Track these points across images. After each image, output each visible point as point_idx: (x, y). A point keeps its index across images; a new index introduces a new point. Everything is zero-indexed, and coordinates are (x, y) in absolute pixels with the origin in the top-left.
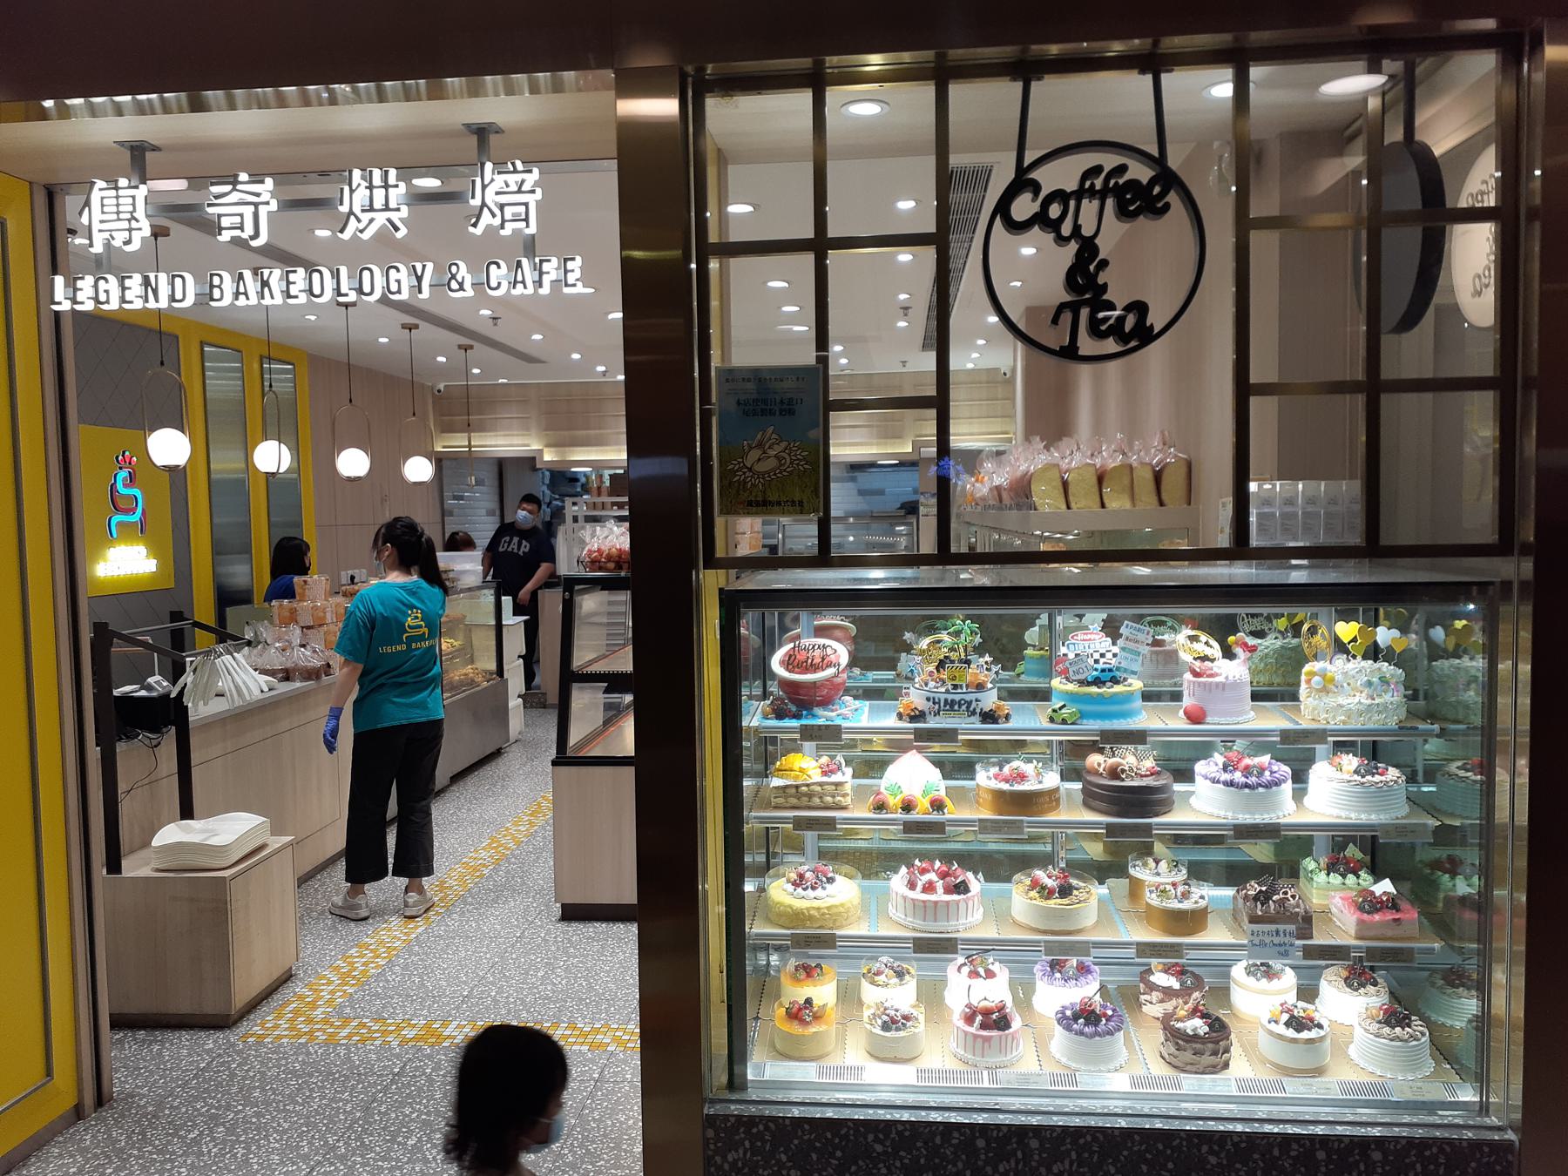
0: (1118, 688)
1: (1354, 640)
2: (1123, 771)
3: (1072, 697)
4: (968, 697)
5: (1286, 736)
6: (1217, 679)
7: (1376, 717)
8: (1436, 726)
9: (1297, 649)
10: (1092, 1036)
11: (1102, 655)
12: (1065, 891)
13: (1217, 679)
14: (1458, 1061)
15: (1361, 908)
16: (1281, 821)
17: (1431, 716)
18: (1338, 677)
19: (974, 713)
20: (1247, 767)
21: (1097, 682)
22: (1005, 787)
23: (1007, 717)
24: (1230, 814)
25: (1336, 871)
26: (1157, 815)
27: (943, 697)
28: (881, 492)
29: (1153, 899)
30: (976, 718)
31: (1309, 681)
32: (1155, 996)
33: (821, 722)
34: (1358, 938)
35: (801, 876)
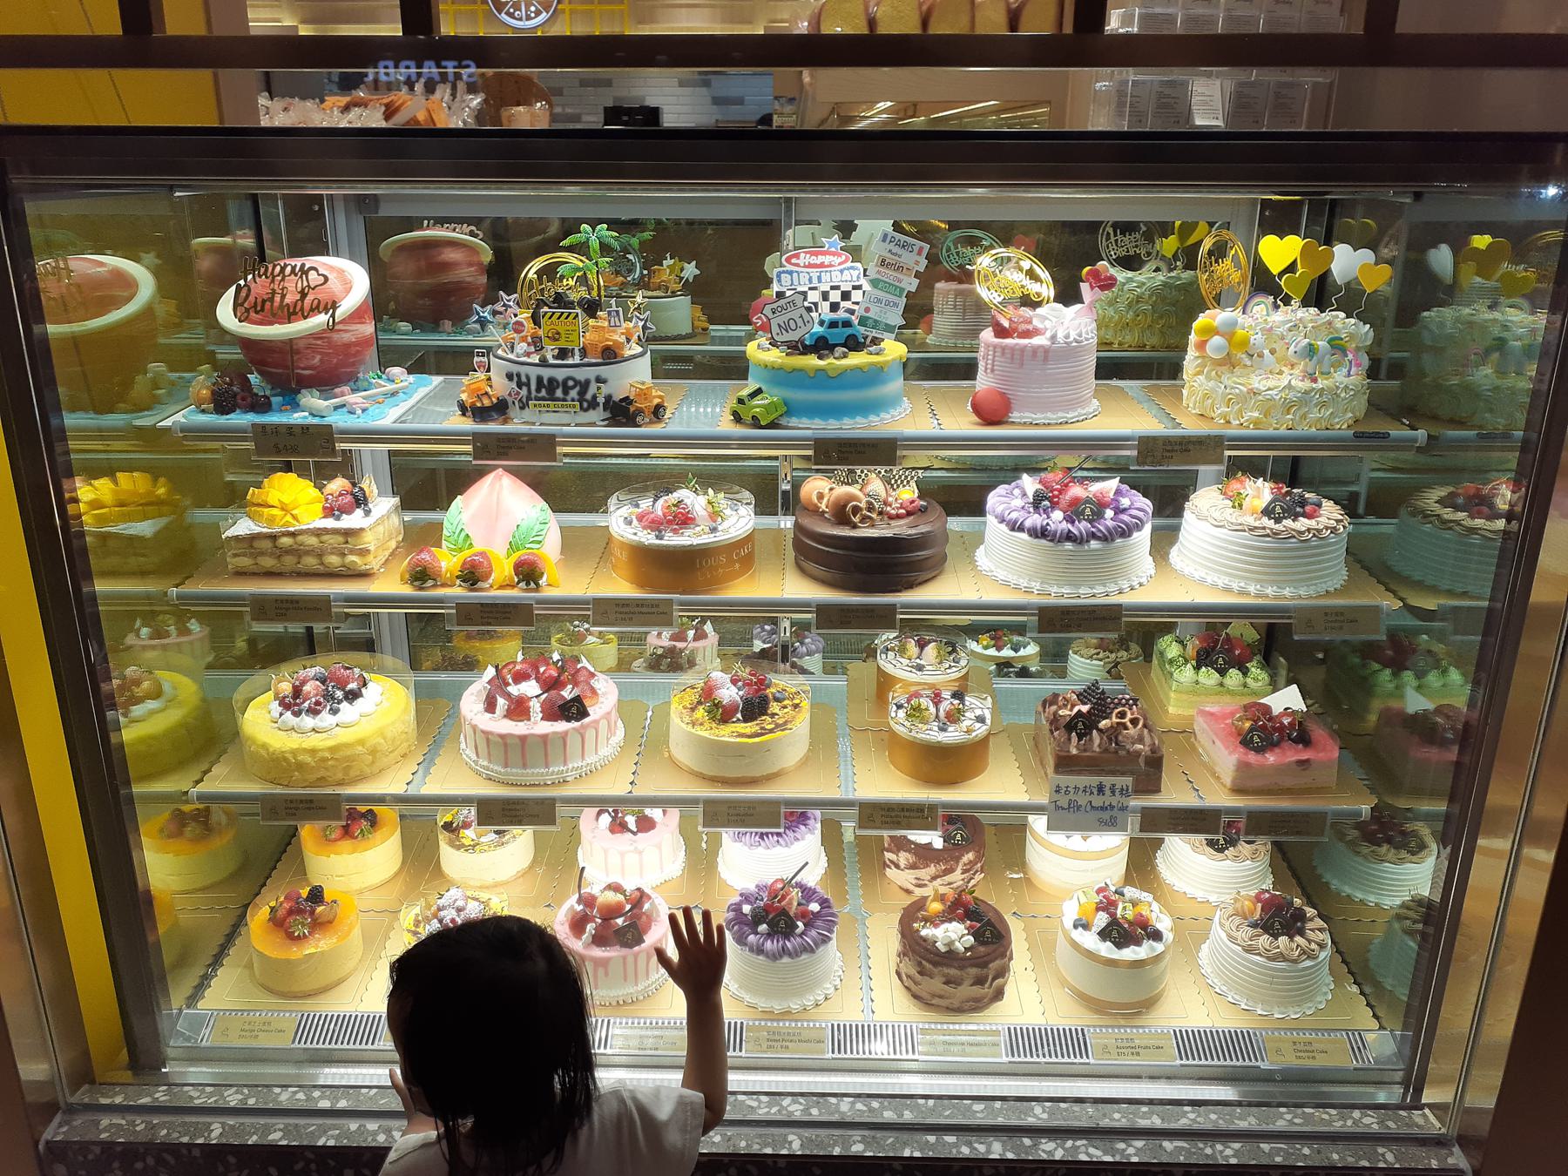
0: (856, 359)
1: (1291, 268)
2: (856, 510)
3: (778, 375)
4: (581, 374)
5: (1150, 447)
6: (1037, 341)
7: (1315, 414)
8: (1421, 434)
9: (1191, 288)
10: (774, 957)
11: (846, 296)
12: (755, 708)
13: (1037, 341)
14: (1377, 985)
15: (1246, 742)
16: (1128, 599)
17: (1409, 411)
18: (1257, 339)
19: (593, 404)
20: (1076, 502)
21: (821, 346)
22: (648, 538)
23: (658, 412)
24: (1036, 586)
25: (1211, 664)
26: (910, 586)
27: (534, 372)
28: (740, 101)
29: (898, 720)
30: (597, 415)
31: (1201, 345)
32: (904, 858)
33: (298, 418)
34: (1238, 790)
35: (297, 692)
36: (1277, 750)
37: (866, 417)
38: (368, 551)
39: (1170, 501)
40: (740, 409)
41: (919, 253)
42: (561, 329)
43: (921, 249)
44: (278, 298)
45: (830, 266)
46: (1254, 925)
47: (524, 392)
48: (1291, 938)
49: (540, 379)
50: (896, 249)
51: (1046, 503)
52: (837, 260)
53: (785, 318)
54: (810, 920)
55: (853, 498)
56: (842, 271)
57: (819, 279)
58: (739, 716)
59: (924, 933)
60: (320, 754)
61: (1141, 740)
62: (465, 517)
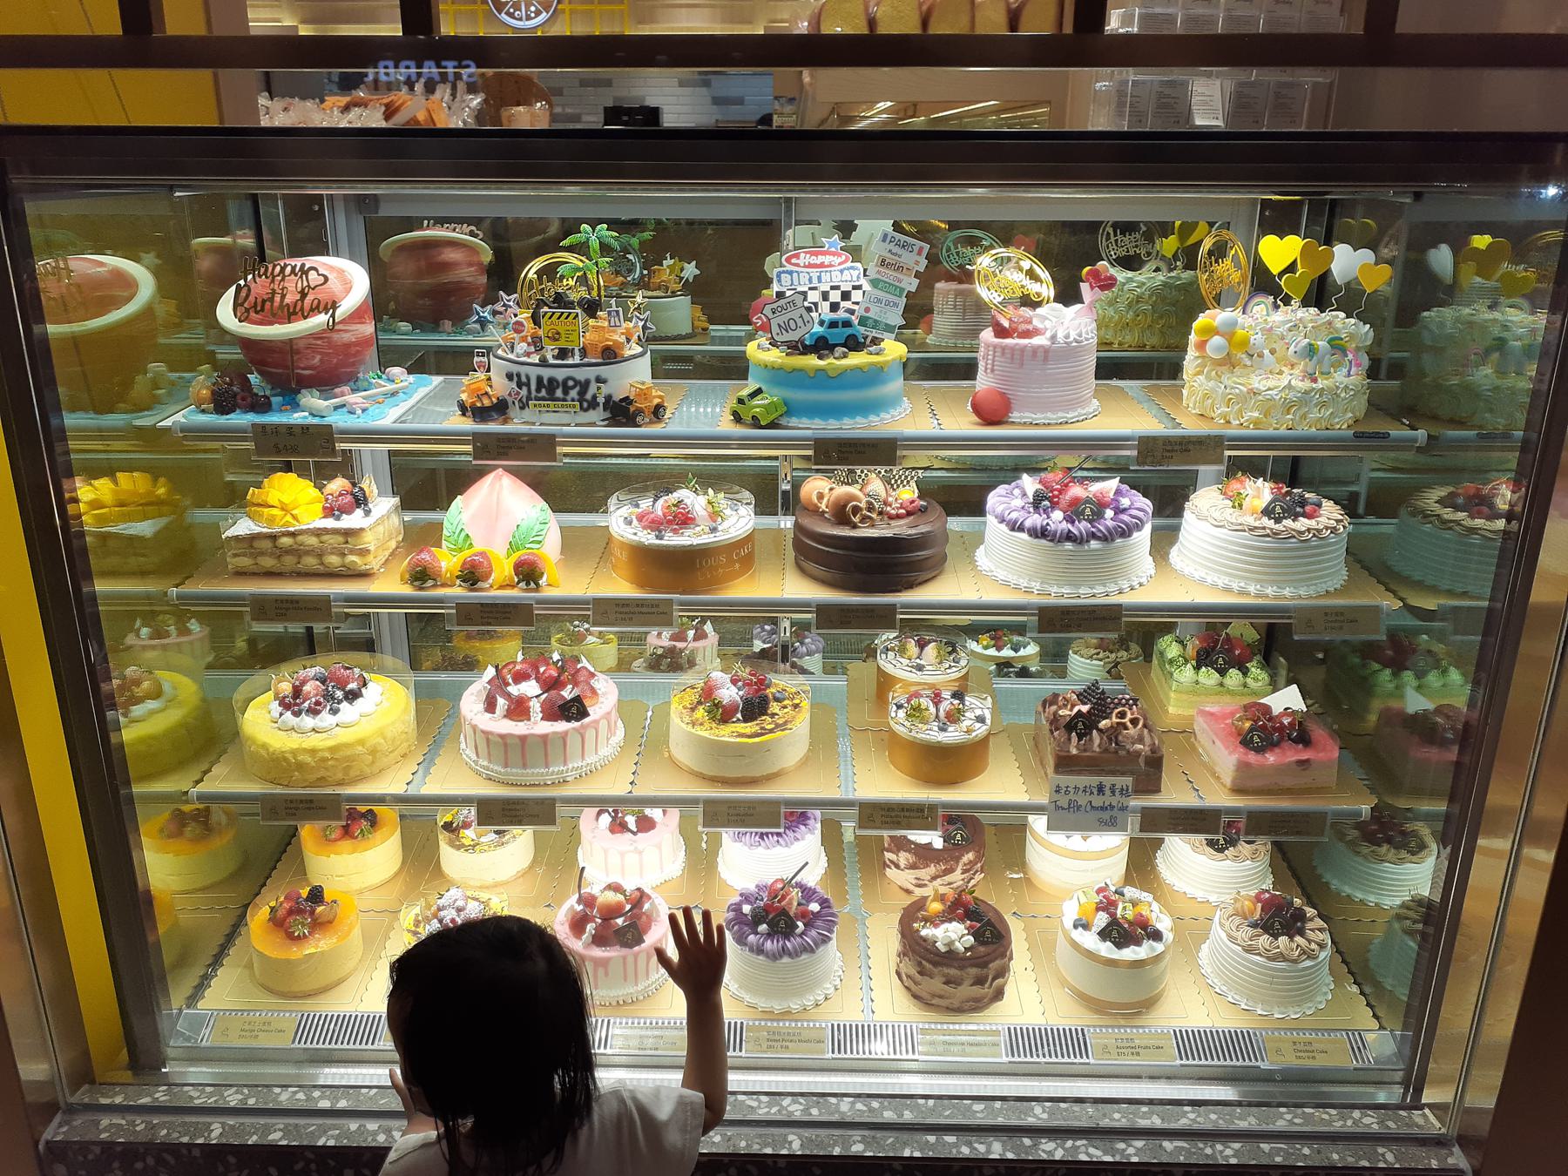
0: (856, 359)
1: (1291, 268)
2: (856, 510)
3: (778, 375)
4: (581, 374)
5: (1150, 447)
6: (1037, 341)
7: (1315, 414)
8: (1421, 434)
9: (1191, 288)
10: (774, 957)
11: (846, 296)
12: (755, 708)
13: (1037, 341)
14: (1377, 985)
15: (1246, 742)
16: (1128, 599)
17: (1409, 411)
18: (1257, 339)
19: (593, 404)
20: (1076, 502)
21: (821, 346)
22: (648, 538)
23: (658, 412)
24: (1036, 586)
25: (1211, 664)
26: (910, 586)
27: (534, 372)
28: (740, 101)
29: (898, 720)
30: (597, 415)
31: (1201, 345)
32: (904, 858)
33: (298, 418)
34: (1238, 790)
35: (297, 692)
36: (1277, 750)
37: (866, 417)
38: (368, 551)
39: (1170, 501)
40: (740, 409)
41: (919, 253)
42: (561, 329)
43: (921, 249)
44: (278, 298)
45: (830, 266)
46: (1254, 925)
47: (524, 392)
48: (1291, 938)
49: (540, 379)
50: (896, 249)
51: (1046, 503)
52: (837, 260)
53: (785, 318)
54: (810, 920)
55: (853, 498)
56: (842, 271)
57: (819, 279)
58: (739, 716)
59: (924, 933)
60: (320, 754)
61: (1141, 740)
62: (465, 517)
